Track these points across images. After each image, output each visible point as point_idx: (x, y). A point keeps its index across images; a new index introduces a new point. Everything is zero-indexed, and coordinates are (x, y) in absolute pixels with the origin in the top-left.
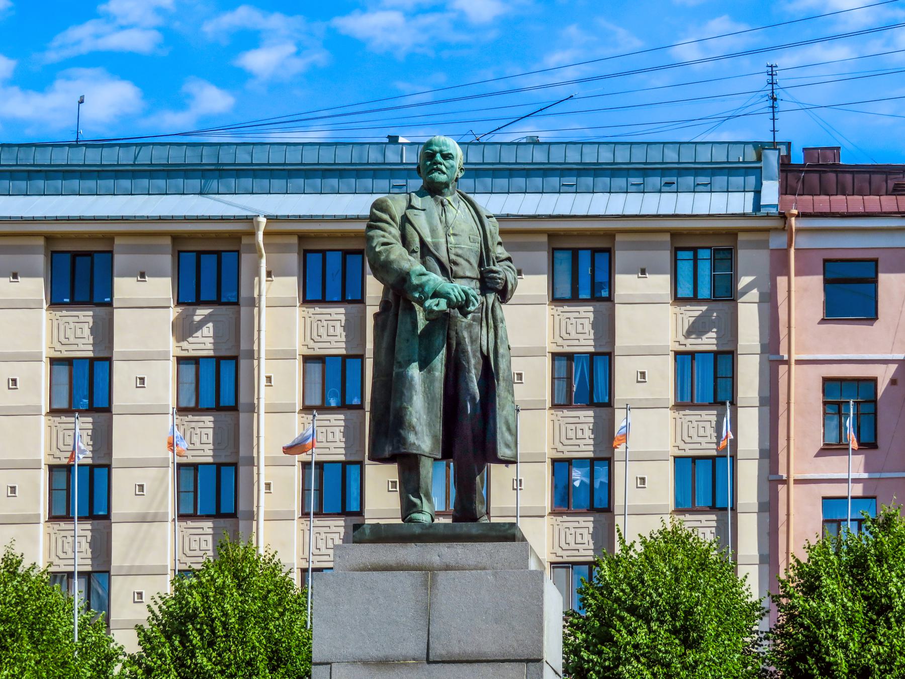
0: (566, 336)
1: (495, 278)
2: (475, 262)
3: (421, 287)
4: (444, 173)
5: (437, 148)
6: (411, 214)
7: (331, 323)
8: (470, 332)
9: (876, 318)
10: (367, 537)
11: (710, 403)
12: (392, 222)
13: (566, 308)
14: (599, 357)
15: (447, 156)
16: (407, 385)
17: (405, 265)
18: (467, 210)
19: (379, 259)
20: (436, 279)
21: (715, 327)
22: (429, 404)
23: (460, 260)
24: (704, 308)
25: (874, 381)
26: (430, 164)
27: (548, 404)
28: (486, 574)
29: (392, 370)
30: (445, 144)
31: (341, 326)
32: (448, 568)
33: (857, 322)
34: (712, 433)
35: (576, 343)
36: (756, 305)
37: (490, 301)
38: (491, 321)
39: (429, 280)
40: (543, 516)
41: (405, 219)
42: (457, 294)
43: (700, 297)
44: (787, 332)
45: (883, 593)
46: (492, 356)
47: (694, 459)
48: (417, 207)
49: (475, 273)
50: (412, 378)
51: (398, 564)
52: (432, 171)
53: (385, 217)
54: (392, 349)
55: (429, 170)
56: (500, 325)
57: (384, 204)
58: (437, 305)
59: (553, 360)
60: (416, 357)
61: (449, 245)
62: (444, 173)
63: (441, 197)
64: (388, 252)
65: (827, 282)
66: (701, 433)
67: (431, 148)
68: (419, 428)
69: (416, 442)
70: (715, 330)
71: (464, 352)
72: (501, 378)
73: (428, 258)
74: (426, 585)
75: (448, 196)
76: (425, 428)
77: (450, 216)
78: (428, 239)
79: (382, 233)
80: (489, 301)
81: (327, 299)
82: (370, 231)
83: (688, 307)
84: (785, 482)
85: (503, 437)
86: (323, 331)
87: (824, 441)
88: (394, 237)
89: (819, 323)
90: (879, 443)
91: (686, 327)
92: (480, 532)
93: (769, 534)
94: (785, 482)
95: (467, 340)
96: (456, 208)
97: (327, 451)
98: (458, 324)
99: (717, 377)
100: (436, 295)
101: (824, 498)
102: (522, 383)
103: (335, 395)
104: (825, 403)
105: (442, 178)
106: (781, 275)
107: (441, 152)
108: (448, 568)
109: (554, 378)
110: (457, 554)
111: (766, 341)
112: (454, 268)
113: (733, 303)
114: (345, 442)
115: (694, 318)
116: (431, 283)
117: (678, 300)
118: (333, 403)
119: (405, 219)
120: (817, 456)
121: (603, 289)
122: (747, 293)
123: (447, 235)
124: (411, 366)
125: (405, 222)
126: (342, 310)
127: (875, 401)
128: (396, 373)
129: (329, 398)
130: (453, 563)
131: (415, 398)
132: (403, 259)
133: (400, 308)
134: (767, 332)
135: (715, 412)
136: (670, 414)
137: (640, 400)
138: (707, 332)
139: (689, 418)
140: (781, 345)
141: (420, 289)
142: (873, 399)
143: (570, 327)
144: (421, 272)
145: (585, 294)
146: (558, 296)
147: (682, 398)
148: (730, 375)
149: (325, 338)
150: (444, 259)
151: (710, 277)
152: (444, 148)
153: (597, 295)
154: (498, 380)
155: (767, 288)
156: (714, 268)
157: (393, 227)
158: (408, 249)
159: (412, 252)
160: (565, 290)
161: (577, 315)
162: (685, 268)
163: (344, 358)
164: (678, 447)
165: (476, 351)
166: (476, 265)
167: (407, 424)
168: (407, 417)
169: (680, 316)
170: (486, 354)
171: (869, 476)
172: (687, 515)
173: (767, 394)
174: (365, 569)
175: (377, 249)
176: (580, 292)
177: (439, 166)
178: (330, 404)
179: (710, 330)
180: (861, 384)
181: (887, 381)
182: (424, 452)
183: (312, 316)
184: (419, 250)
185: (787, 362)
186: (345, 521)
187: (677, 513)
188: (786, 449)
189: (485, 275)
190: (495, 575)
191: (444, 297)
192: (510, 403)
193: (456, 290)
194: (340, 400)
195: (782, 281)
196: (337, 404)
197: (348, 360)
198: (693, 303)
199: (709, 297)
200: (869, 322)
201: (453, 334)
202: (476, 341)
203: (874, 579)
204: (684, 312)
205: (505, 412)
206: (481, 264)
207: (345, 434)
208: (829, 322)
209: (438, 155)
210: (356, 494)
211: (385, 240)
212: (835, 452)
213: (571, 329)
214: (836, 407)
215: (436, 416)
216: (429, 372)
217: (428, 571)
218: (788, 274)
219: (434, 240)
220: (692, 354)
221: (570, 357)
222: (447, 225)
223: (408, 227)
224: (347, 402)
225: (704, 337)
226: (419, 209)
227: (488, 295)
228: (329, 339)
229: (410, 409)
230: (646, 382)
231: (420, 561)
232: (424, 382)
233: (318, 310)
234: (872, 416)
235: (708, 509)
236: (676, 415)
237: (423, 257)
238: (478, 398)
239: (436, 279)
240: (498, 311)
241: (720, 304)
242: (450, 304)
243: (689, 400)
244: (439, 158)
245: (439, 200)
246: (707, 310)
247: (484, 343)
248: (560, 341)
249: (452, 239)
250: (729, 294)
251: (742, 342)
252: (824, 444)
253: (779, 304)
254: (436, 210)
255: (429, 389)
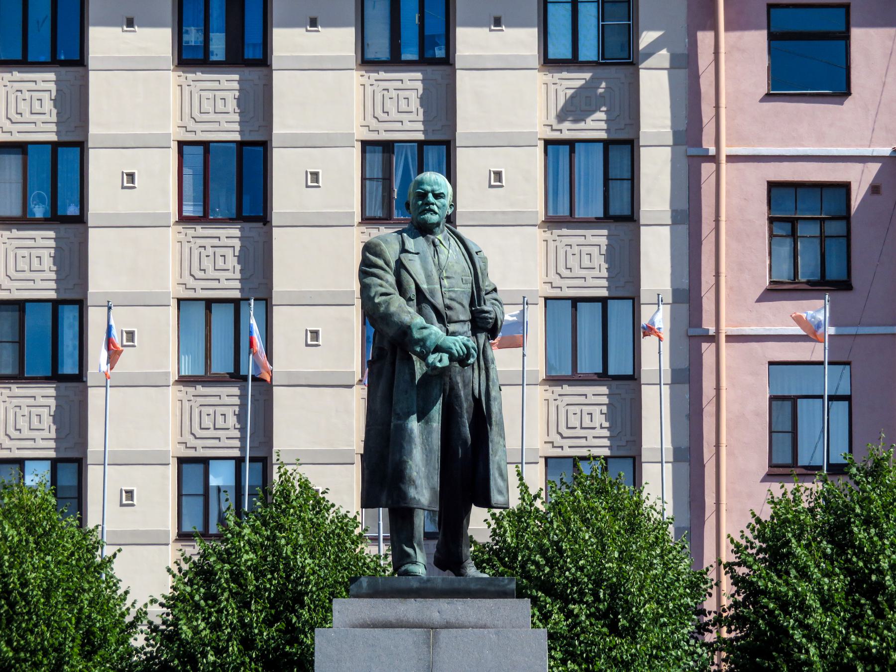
0: (383, 117)
1: (486, 318)
2: (466, 303)
3: (422, 341)
4: (436, 213)
5: (429, 188)
6: (404, 256)
7: (36, 95)
8: (463, 376)
9: (847, 93)
10: (364, 591)
11: (597, 218)
12: (387, 269)
13: (383, 75)
14: (430, 147)
15: (438, 196)
16: (407, 438)
17: (406, 318)
18: (457, 248)
19: (378, 310)
20: (436, 332)
21: (605, 105)
22: (427, 456)
23: (454, 304)
24: (588, 75)
25: (846, 187)
26: (422, 204)
27: (358, 218)
28: (489, 632)
29: (390, 422)
30: (437, 183)
31: (51, 100)
32: (448, 626)
33: (820, 99)
34: (603, 263)
35: (398, 126)
36: (666, 72)
37: (482, 341)
38: (482, 363)
39: (430, 334)
40: (351, 386)
41: (400, 265)
42: (459, 348)
43: (582, 58)
44: (714, 114)
45: (873, 567)
46: (483, 398)
47: (575, 301)
48: (411, 251)
49: (465, 315)
50: (412, 431)
51: (397, 620)
52: (424, 212)
53: (380, 262)
54: (389, 398)
55: (420, 210)
56: (492, 366)
57: (378, 249)
58: (440, 361)
59: (364, 151)
60: (415, 408)
61: (443, 290)
62: (436, 213)
63: (432, 237)
64: (388, 304)
65: (772, 37)
66: (586, 262)
67: (422, 187)
68: (418, 482)
69: (416, 496)
70: (604, 109)
71: (458, 397)
72: (494, 423)
73: (424, 305)
74: (428, 644)
75: (439, 234)
76: (423, 481)
77: (443, 257)
78: (424, 286)
79: (379, 281)
80: (479, 341)
81: (30, 59)
82: (365, 278)
83: (565, 75)
84: (714, 339)
85: (496, 484)
86: (24, 107)
87: (770, 277)
88: (391, 285)
89: (762, 101)
90: (855, 282)
91: (561, 102)
92: (479, 587)
93: (689, 417)
94: (714, 339)
95: (460, 385)
96: (447, 247)
97: (30, 284)
98: (452, 370)
99: (609, 179)
100: (438, 349)
101: (771, 363)
102: (319, 187)
103: (41, 200)
104: (771, 220)
105: (434, 218)
106: (704, 28)
107: (433, 192)
108: (448, 626)
109: (366, 179)
110: (458, 610)
111: (682, 127)
112: (449, 313)
113: (630, 69)
114: (57, 272)
115: (572, 91)
116: (433, 337)
117: (549, 62)
118: (39, 211)
119: (400, 265)
120: (760, 300)
121: (438, 45)
122: (654, 54)
123: (441, 279)
124: (410, 419)
125: (400, 268)
126: (52, 76)
127: (846, 217)
128: (394, 425)
129: (32, 206)
130: (453, 620)
131: (415, 451)
132: (403, 311)
133: (398, 358)
134: (683, 113)
135: (605, 232)
136: (539, 234)
137: (495, 213)
138: (594, 111)
139: (566, 240)
140: (704, 133)
141: (422, 343)
142: (844, 214)
143: (388, 102)
144: (422, 326)
145: (410, 54)
146: (370, 55)
147: (555, 209)
148: (627, 175)
149: (27, 116)
150: (441, 306)
151: (596, 29)
152: (436, 187)
153: (428, 55)
154: (491, 425)
155: (682, 48)
156: (602, 15)
157: (389, 273)
158: (404, 298)
159: (409, 300)
160: (380, 48)
161: (398, 84)
162: (560, 15)
163: (55, 146)
164: (551, 283)
165: (469, 395)
166: (467, 307)
167: (407, 478)
168: (408, 471)
169: (552, 88)
170: (477, 397)
171: (836, 330)
172: (565, 387)
173: (684, 205)
174: (365, 625)
175: (377, 300)
176: (402, 50)
177: (431, 206)
178: (34, 214)
179: (597, 109)
180: (826, 192)
181: (865, 187)
182: (423, 505)
183: (8, 84)
184: (415, 298)
185: (715, 159)
186: (56, 389)
187: (551, 383)
188: (714, 288)
189: (476, 315)
190: (497, 634)
191: (447, 352)
192: (502, 447)
193: (457, 344)
194: (49, 208)
195: (705, 38)
196: (44, 214)
197: (60, 149)
198: (572, 68)
199: (595, 59)
200: (838, 99)
201: (447, 379)
202: (468, 385)
203: (861, 548)
204: (558, 81)
205: (497, 458)
206: (472, 304)
207: (57, 260)
208: (776, 98)
209: (430, 195)
210: (70, 349)
211: (383, 290)
212: (787, 294)
213: (390, 106)
214: (788, 226)
215: (434, 468)
216: (427, 423)
217: (430, 627)
218: (715, 28)
219: (429, 287)
220: (571, 144)
221: (387, 147)
222: (440, 268)
223: (404, 274)
224: (60, 212)
225: (589, 120)
226: (413, 253)
227: (479, 335)
228: (34, 118)
229: (410, 462)
230: (502, 186)
231: (420, 617)
232: (422, 433)
233: (17, 75)
234: (844, 241)
235: (595, 377)
236: (547, 235)
237: (418, 304)
238: (470, 442)
239: (436, 332)
240: (489, 352)
241: (613, 69)
242: (452, 358)
243: (567, 213)
244: (431, 198)
245: (431, 240)
246: (592, 78)
247: (476, 386)
248: (374, 124)
249: (445, 282)
250: (626, 55)
251: (646, 127)
252: (771, 282)
253: (700, 72)
254: (429, 251)
255: (427, 440)
